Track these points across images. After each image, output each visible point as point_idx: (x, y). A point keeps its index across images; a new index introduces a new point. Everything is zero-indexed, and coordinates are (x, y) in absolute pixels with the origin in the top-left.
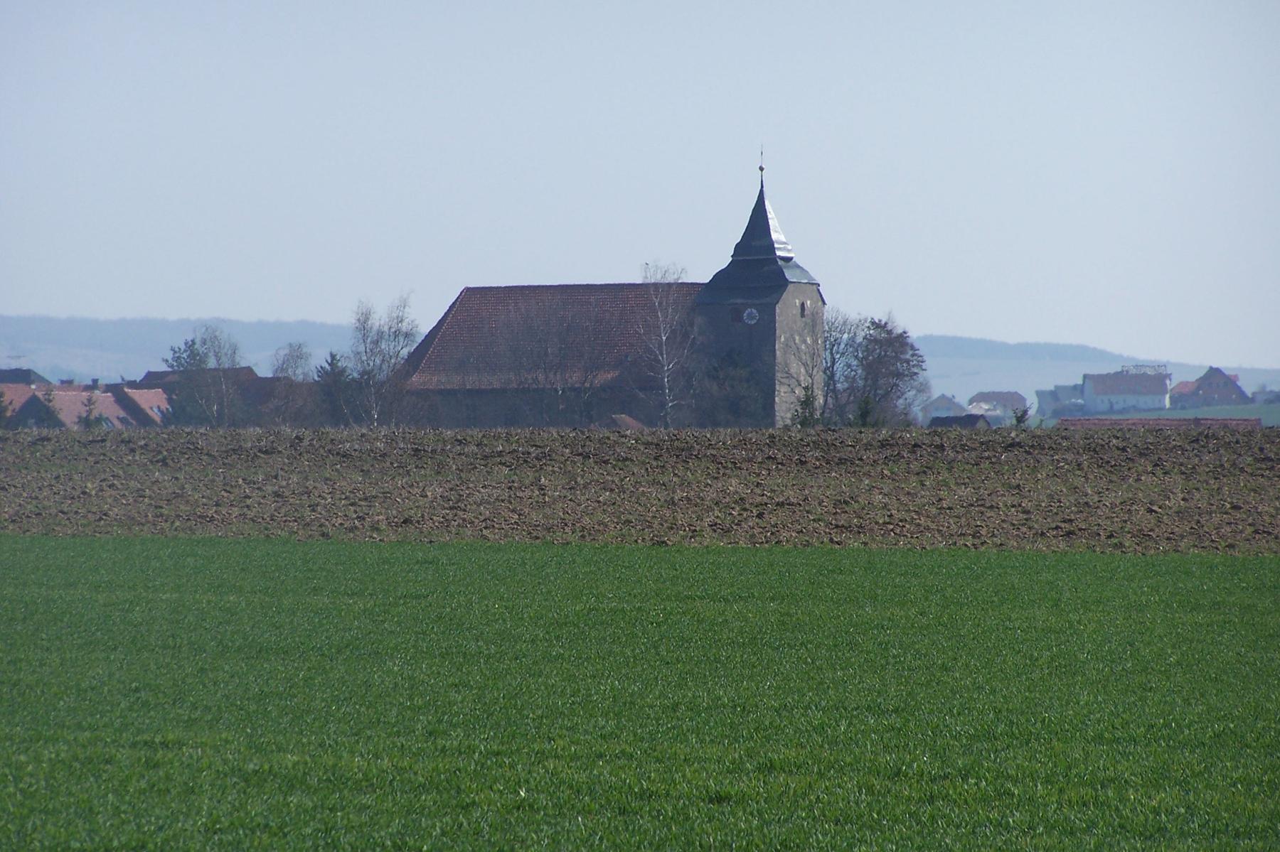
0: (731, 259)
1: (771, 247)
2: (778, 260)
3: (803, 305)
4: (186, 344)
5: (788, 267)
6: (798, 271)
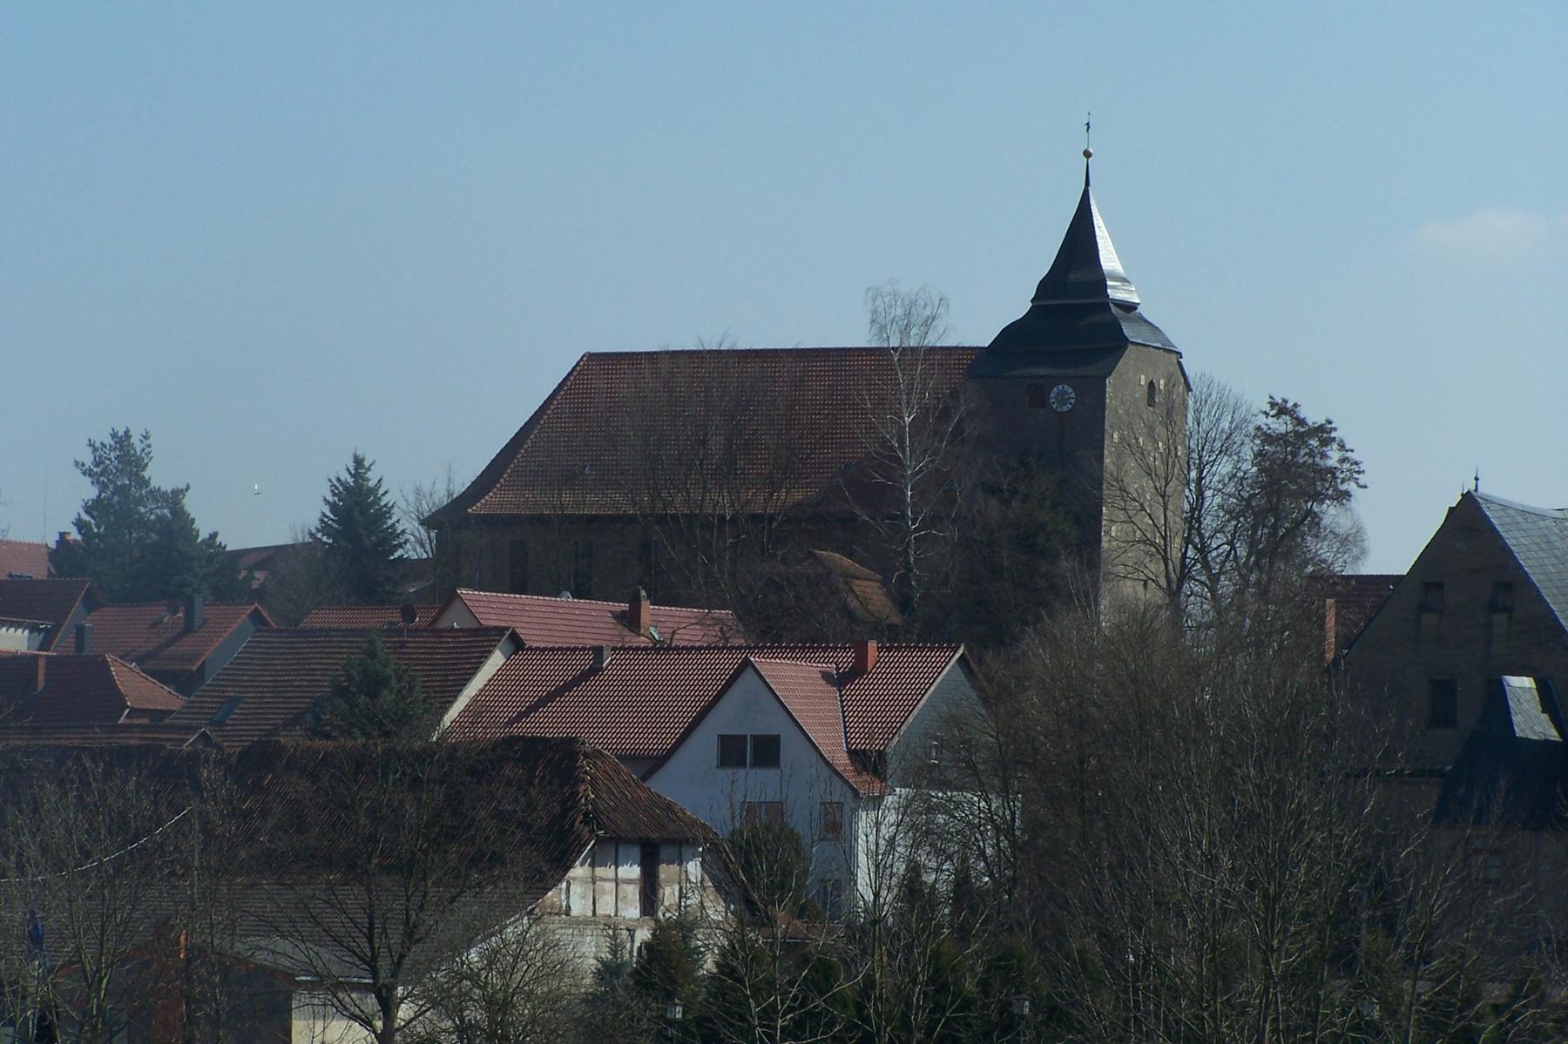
0: (1031, 305)
1: (1098, 281)
2: (1111, 305)
3: (1151, 385)
4: (114, 435)
5: (1128, 320)
6: (1144, 329)
